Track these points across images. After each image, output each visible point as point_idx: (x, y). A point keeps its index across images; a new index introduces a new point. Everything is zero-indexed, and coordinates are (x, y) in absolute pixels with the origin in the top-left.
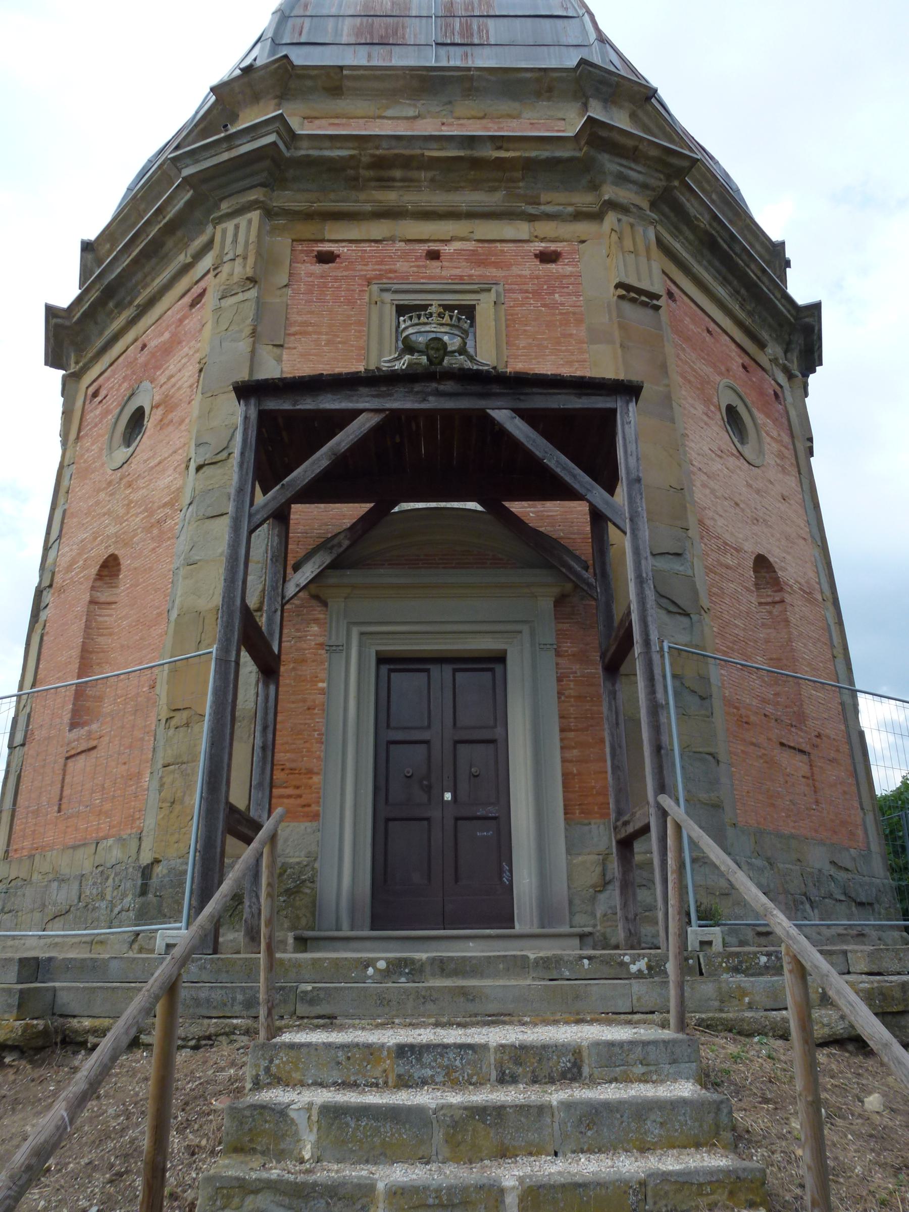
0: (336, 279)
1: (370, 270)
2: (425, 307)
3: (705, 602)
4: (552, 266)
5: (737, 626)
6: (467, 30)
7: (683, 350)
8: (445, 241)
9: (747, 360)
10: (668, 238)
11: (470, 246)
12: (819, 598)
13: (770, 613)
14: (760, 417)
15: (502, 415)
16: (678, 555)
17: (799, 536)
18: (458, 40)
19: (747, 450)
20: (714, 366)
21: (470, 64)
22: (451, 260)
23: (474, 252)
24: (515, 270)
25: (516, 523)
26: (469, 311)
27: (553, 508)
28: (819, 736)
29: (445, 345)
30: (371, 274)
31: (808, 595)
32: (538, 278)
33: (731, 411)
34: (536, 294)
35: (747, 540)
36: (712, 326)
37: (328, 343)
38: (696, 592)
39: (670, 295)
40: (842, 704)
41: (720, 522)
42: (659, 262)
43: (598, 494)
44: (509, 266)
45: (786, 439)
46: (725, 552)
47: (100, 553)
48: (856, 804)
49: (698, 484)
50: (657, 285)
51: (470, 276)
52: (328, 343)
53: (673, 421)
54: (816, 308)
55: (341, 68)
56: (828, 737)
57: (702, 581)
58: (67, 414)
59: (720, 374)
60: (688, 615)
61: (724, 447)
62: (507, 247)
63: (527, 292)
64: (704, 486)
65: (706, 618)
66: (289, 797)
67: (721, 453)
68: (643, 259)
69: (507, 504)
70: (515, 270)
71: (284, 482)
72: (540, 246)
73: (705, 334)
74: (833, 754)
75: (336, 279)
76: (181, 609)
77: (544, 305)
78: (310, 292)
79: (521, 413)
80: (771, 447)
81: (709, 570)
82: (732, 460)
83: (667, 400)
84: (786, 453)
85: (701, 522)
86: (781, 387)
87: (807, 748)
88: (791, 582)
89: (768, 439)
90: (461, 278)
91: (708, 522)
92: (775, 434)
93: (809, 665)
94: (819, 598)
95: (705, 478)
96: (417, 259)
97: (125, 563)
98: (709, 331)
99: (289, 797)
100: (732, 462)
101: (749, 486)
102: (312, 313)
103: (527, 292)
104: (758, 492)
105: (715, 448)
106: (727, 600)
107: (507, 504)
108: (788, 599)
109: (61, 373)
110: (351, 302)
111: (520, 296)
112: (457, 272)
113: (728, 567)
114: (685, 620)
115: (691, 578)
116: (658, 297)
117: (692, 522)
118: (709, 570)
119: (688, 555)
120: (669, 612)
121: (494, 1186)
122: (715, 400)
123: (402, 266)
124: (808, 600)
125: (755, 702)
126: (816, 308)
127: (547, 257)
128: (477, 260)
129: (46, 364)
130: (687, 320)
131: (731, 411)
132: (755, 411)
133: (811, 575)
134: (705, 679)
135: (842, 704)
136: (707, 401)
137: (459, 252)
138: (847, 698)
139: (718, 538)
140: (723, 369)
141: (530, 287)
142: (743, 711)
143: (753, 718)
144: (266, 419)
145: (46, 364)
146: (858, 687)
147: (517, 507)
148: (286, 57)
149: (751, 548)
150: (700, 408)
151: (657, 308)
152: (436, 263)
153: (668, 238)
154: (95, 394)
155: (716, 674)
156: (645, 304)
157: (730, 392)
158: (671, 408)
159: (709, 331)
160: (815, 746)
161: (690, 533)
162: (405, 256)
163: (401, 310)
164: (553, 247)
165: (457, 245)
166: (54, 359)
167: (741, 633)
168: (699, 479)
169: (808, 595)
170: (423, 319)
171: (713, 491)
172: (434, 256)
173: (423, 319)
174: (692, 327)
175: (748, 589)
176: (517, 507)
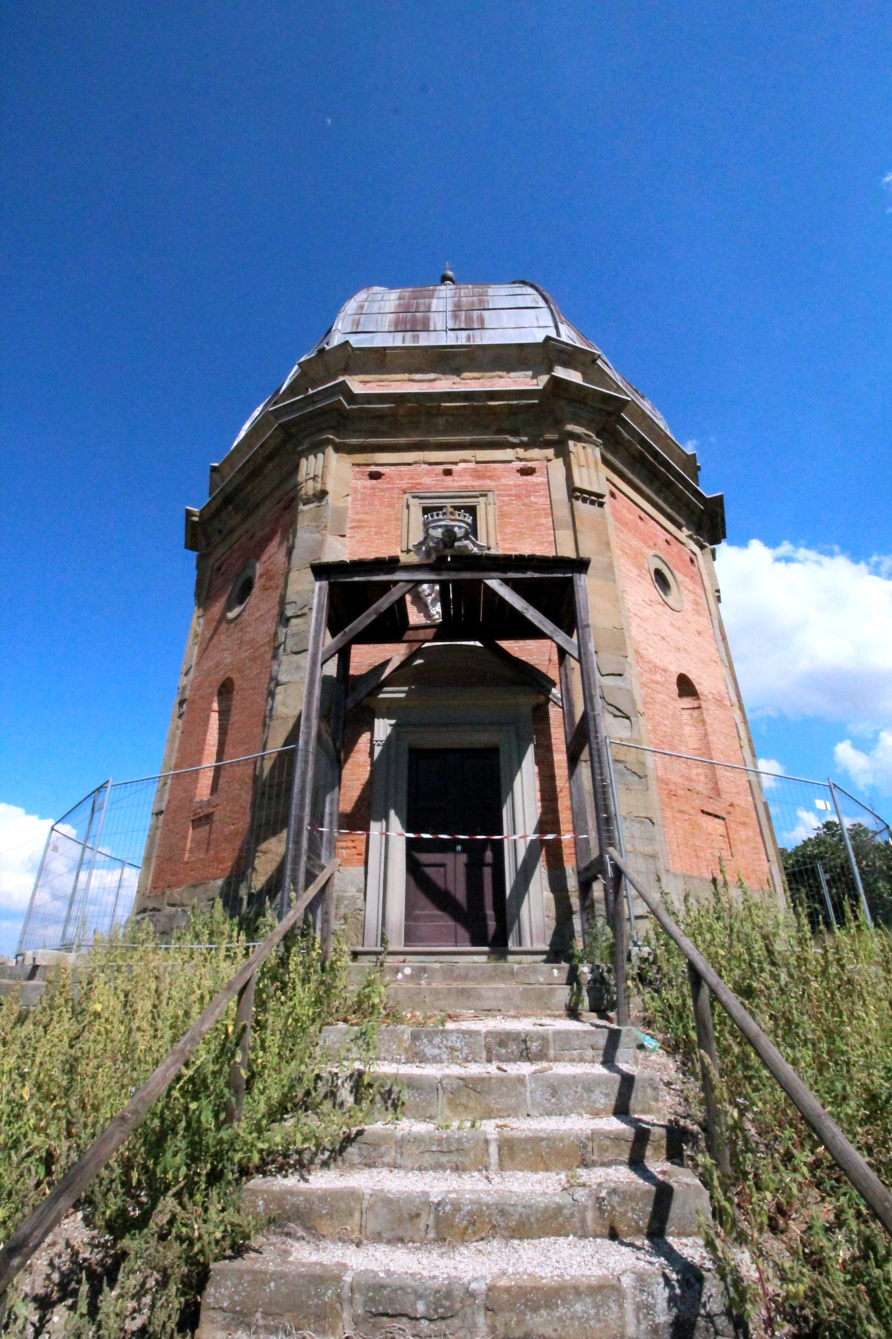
0: (382, 490)
1: (405, 483)
2: (440, 508)
3: (640, 707)
4: (529, 478)
5: (665, 725)
6: (469, 319)
7: (622, 532)
8: (456, 463)
9: (669, 537)
10: (610, 457)
11: (472, 465)
12: (728, 704)
13: (691, 715)
14: (680, 577)
15: (494, 584)
16: (620, 675)
17: (712, 660)
18: (463, 326)
19: (670, 600)
20: (645, 542)
21: (472, 343)
22: (460, 475)
23: (475, 471)
24: (504, 481)
25: (505, 655)
26: (472, 510)
27: (531, 645)
28: (732, 805)
29: (455, 533)
30: (404, 486)
31: (719, 702)
32: (519, 486)
33: (658, 574)
34: (518, 496)
35: (671, 663)
36: (643, 514)
37: (377, 533)
38: (634, 702)
39: (613, 495)
40: (749, 782)
41: (651, 651)
42: (606, 472)
43: (561, 637)
44: (499, 478)
45: (700, 591)
46: (656, 672)
47: (218, 678)
48: (764, 857)
49: (634, 624)
50: (602, 488)
51: (473, 486)
52: (377, 533)
53: (615, 582)
54: (719, 501)
55: (385, 348)
56: (739, 806)
57: (639, 694)
58: (199, 583)
59: (649, 547)
60: (628, 718)
61: (653, 598)
62: (497, 465)
63: (511, 495)
64: (639, 626)
65: (642, 720)
66: (347, 848)
67: (651, 603)
68: (593, 472)
69: (499, 642)
70: (504, 481)
71: (347, 629)
72: (521, 464)
73: (638, 520)
74: (743, 819)
75: (382, 490)
76: (579, 873)
77: (524, 504)
78: (364, 499)
79: (506, 582)
80: (688, 597)
81: (644, 685)
82: (659, 607)
83: (611, 566)
84: (700, 601)
85: (637, 652)
86: (695, 554)
87: (723, 814)
88: (706, 693)
89: (686, 592)
90: (466, 487)
91: (643, 652)
92: (691, 587)
93: (722, 752)
94: (728, 704)
95: (638, 620)
96: (437, 475)
97: (238, 683)
98: (641, 518)
99: (347, 848)
100: (660, 609)
101: (672, 625)
102: (366, 513)
103: (511, 495)
104: (679, 629)
105: (646, 599)
106: (658, 707)
107: (499, 642)
108: (704, 705)
109: (196, 554)
110: (391, 505)
111: (506, 499)
112: (464, 483)
113: (657, 683)
114: (627, 721)
115: (629, 692)
116: (602, 496)
117: (630, 651)
118: (644, 685)
119: (626, 674)
120: (615, 716)
121: (528, 1216)
122: (646, 566)
123: (427, 480)
124: (720, 706)
125: (680, 780)
126: (719, 501)
127: (526, 472)
128: (477, 474)
129: (186, 547)
130: (625, 511)
131: (658, 574)
132: (675, 572)
133: (722, 687)
134: (643, 764)
135: (749, 782)
136: (640, 567)
137: (465, 470)
138: (752, 777)
139: (650, 662)
140: (652, 544)
141: (513, 492)
142: (672, 787)
143: (680, 792)
144: (334, 589)
145: (186, 547)
146: (760, 770)
147: (505, 644)
148: (347, 342)
149: (675, 670)
150: (635, 572)
151: (601, 505)
152: (449, 478)
153: (610, 457)
154: (219, 569)
155: (650, 760)
156: (592, 503)
157: (657, 560)
158: (613, 572)
159: (641, 518)
160: (729, 813)
161: (629, 659)
162: (428, 473)
163: (426, 510)
164: (530, 464)
165: (462, 465)
166: (191, 545)
167: (669, 730)
168: (634, 622)
169: (719, 702)
170: (441, 517)
171: (645, 630)
172: (448, 473)
173: (441, 517)
174: (628, 515)
175: (673, 699)
176: (505, 644)
